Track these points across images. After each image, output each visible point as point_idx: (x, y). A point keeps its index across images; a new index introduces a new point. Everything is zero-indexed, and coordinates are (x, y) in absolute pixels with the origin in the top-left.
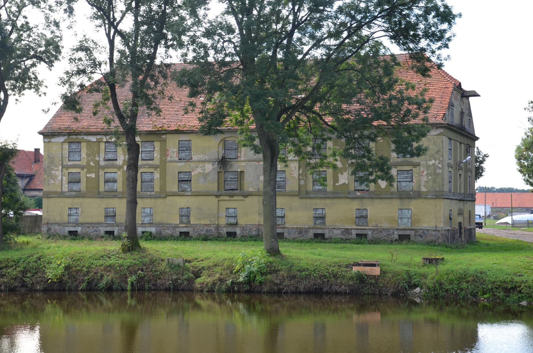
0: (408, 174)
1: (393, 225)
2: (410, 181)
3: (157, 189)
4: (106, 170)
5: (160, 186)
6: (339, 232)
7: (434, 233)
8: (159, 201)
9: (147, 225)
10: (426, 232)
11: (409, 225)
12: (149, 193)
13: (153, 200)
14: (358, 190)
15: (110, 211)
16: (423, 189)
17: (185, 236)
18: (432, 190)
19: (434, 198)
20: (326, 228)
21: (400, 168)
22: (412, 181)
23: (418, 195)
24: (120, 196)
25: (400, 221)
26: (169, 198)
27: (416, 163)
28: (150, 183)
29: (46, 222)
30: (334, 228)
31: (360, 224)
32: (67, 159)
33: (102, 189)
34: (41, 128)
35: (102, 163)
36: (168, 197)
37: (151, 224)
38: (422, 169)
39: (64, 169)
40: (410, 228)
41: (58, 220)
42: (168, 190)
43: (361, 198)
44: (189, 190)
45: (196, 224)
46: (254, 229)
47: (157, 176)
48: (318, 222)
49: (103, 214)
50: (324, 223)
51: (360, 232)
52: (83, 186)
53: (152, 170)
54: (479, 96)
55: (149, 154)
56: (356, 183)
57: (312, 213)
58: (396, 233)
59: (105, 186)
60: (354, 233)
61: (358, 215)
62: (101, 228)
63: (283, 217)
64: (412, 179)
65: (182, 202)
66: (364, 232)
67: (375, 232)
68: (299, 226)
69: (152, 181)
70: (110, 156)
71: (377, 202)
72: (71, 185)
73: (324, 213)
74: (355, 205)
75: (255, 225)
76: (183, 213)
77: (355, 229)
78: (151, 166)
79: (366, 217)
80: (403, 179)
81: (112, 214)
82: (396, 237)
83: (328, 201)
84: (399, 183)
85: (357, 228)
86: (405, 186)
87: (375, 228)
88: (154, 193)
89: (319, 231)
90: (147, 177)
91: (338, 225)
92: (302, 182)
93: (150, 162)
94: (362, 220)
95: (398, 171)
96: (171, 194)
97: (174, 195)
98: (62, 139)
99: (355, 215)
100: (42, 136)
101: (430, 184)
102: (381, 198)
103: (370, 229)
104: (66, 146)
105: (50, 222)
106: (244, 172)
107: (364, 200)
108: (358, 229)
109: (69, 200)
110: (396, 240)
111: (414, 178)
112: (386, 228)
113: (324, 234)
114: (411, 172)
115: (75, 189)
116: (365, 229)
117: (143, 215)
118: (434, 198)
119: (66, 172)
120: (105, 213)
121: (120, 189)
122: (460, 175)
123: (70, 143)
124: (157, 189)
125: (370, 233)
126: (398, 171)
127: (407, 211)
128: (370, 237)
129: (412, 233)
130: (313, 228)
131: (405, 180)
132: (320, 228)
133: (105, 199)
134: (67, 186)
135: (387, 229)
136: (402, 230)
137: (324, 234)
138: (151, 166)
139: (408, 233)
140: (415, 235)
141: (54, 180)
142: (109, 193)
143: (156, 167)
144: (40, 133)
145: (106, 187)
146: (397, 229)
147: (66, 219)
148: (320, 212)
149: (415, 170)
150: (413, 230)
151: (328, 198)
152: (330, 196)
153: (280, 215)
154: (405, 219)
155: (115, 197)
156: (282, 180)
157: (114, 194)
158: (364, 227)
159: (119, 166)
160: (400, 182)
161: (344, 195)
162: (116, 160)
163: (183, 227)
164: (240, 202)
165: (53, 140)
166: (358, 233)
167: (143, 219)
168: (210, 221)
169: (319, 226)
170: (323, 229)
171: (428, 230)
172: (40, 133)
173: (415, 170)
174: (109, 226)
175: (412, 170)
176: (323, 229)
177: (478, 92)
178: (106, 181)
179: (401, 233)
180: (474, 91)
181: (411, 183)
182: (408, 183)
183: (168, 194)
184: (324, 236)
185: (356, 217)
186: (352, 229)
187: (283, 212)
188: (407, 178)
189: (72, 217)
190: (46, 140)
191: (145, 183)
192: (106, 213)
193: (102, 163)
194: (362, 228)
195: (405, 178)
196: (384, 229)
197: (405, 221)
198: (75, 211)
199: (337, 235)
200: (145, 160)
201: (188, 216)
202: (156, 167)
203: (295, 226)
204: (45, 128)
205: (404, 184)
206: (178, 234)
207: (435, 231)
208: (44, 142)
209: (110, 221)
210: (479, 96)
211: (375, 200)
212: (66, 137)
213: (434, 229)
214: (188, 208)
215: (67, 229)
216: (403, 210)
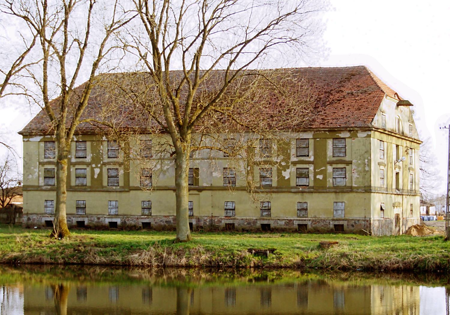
0: (342, 171)
1: (329, 216)
2: (344, 178)
3: (121, 184)
4: (77, 167)
5: (124, 182)
6: (284, 222)
7: (363, 222)
8: (124, 195)
9: (113, 216)
10: (357, 222)
11: (343, 216)
12: (114, 188)
13: (118, 194)
14: (300, 186)
15: (81, 203)
16: (354, 185)
17: (266, 229)
18: (362, 185)
19: (364, 192)
20: (272, 220)
21: (335, 166)
22: (346, 177)
23: (350, 190)
24: (89, 190)
25: (335, 213)
26: (132, 192)
27: (349, 161)
28: (115, 179)
29: (26, 212)
30: (279, 220)
31: (301, 215)
32: (43, 156)
33: (105, 184)
34: (21, 129)
35: (74, 160)
36: (131, 191)
37: (117, 216)
38: (354, 167)
39: (40, 166)
40: (343, 218)
41: (36, 211)
42: (132, 184)
43: (302, 192)
44: (150, 185)
45: (156, 216)
46: (208, 220)
47: (121, 172)
48: (265, 214)
49: (75, 206)
50: (270, 215)
51: (301, 223)
52: (88, 182)
53: (115, 167)
54: (412, 105)
55: (115, 152)
56: (297, 179)
57: (259, 206)
58: (331, 223)
59: (76, 181)
60: (296, 223)
61: (300, 208)
62: (74, 219)
63: (234, 209)
64: (346, 176)
65: (145, 195)
66: (304, 223)
67: (314, 223)
68: (248, 218)
69: (116, 176)
70: (81, 154)
71: (315, 195)
72: (47, 180)
73: (270, 206)
74: (298, 198)
75: (208, 216)
76: (145, 206)
77: (297, 220)
78: (115, 163)
79: (306, 210)
80: (338, 175)
81: (82, 206)
82: (332, 226)
83: (274, 195)
84: (334, 180)
85: (298, 219)
86: (339, 182)
87: (314, 219)
88: (119, 187)
89: (265, 222)
90: (113, 173)
91: (282, 216)
92: (250, 178)
93: (115, 160)
94: (303, 212)
95: (333, 168)
96: (134, 189)
97: (137, 189)
98: (38, 138)
99: (296, 208)
100: (22, 136)
101: (361, 180)
102: (319, 192)
103: (310, 220)
104: (42, 144)
105: (30, 212)
106: (198, 169)
107: (305, 194)
108: (299, 220)
109: (46, 193)
110: (43, 226)
111: (347, 175)
112: (323, 219)
113: (270, 225)
114: (345, 169)
115: (50, 183)
116: (305, 220)
117: (109, 207)
118: (364, 192)
119: (42, 168)
120: (77, 205)
121: (89, 184)
122: (397, 174)
123: (46, 142)
124: (121, 184)
125: (309, 223)
126: (297, 168)
127: (341, 204)
128: (309, 227)
129: (345, 223)
130: (260, 219)
131: (339, 176)
132: (266, 220)
133: (76, 192)
134: (43, 181)
135: (324, 220)
136: (337, 220)
137: (270, 225)
138: (115, 163)
139: (341, 223)
140: (348, 225)
141: (32, 175)
142: (80, 187)
143: (120, 164)
144: (20, 133)
145: (78, 182)
146: (333, 220)
147: (43, 210)
148: (266, 204)
149: (348, 168)
150: (346, 220)
151: (273, 192)
152: (275, 190)
153: (231, 208)
154: (339, 211)
155: (85, 191)
156: (232, 176)
157: (84, 188)
158: (304, 219)
159: (88, 163)
160: (335, 178)
161: (286, 190)
162: (86, 157)
163: (145, 218)
164: (196, 196)
165: (31, 139)
166: (299, 223)
167: (109, 211)
168: (169, 213)
169: (265, 218)
170: (269, 220)
171: (359, 220)
172: (20, 133)
173: (348, 168)
174: (79, 217)
175: (345, 168)
176: (269, 220)
177: (411, 103)
178: (77, 177)
179: (337, 223)
180: (408, 101)
181: (345, 179)
182: (342, 179)
183: (131, 189)
184: (343, 228)
185: (298, 210)
186: (294, 220)
187: (234, 205)
188: (341, 175)
189: (48, 209)
190: (26, 140)
191: (111, 179)
192: (77, 204)
193: (74, 160)
194: (302, 219)
195: (340, 175)
196: (322, 220)
197: (340, 212)
198: (50, 203)
199: (280, 225)
200: (111, 158)
201: (150, 209)
202: (120, 164)
203: (245, 218)
204: (25, 129)
205: (338, 180)
206: (141, 225)
207: (364, 221)
208: (24, 141)
209: (81, 212)
210: (412, 105)
211: (314, 195)
212: (42, 137)
213: (364, 219)
214: (149, 201)
215: (44, 219)
216: (338, 203)
